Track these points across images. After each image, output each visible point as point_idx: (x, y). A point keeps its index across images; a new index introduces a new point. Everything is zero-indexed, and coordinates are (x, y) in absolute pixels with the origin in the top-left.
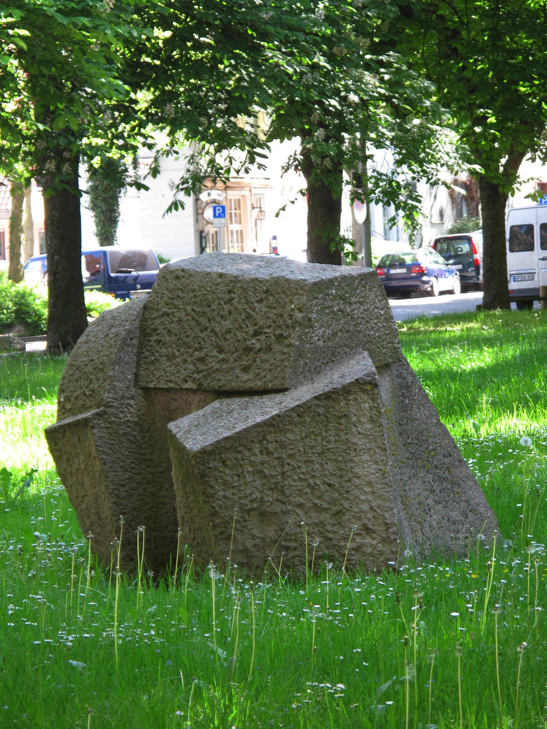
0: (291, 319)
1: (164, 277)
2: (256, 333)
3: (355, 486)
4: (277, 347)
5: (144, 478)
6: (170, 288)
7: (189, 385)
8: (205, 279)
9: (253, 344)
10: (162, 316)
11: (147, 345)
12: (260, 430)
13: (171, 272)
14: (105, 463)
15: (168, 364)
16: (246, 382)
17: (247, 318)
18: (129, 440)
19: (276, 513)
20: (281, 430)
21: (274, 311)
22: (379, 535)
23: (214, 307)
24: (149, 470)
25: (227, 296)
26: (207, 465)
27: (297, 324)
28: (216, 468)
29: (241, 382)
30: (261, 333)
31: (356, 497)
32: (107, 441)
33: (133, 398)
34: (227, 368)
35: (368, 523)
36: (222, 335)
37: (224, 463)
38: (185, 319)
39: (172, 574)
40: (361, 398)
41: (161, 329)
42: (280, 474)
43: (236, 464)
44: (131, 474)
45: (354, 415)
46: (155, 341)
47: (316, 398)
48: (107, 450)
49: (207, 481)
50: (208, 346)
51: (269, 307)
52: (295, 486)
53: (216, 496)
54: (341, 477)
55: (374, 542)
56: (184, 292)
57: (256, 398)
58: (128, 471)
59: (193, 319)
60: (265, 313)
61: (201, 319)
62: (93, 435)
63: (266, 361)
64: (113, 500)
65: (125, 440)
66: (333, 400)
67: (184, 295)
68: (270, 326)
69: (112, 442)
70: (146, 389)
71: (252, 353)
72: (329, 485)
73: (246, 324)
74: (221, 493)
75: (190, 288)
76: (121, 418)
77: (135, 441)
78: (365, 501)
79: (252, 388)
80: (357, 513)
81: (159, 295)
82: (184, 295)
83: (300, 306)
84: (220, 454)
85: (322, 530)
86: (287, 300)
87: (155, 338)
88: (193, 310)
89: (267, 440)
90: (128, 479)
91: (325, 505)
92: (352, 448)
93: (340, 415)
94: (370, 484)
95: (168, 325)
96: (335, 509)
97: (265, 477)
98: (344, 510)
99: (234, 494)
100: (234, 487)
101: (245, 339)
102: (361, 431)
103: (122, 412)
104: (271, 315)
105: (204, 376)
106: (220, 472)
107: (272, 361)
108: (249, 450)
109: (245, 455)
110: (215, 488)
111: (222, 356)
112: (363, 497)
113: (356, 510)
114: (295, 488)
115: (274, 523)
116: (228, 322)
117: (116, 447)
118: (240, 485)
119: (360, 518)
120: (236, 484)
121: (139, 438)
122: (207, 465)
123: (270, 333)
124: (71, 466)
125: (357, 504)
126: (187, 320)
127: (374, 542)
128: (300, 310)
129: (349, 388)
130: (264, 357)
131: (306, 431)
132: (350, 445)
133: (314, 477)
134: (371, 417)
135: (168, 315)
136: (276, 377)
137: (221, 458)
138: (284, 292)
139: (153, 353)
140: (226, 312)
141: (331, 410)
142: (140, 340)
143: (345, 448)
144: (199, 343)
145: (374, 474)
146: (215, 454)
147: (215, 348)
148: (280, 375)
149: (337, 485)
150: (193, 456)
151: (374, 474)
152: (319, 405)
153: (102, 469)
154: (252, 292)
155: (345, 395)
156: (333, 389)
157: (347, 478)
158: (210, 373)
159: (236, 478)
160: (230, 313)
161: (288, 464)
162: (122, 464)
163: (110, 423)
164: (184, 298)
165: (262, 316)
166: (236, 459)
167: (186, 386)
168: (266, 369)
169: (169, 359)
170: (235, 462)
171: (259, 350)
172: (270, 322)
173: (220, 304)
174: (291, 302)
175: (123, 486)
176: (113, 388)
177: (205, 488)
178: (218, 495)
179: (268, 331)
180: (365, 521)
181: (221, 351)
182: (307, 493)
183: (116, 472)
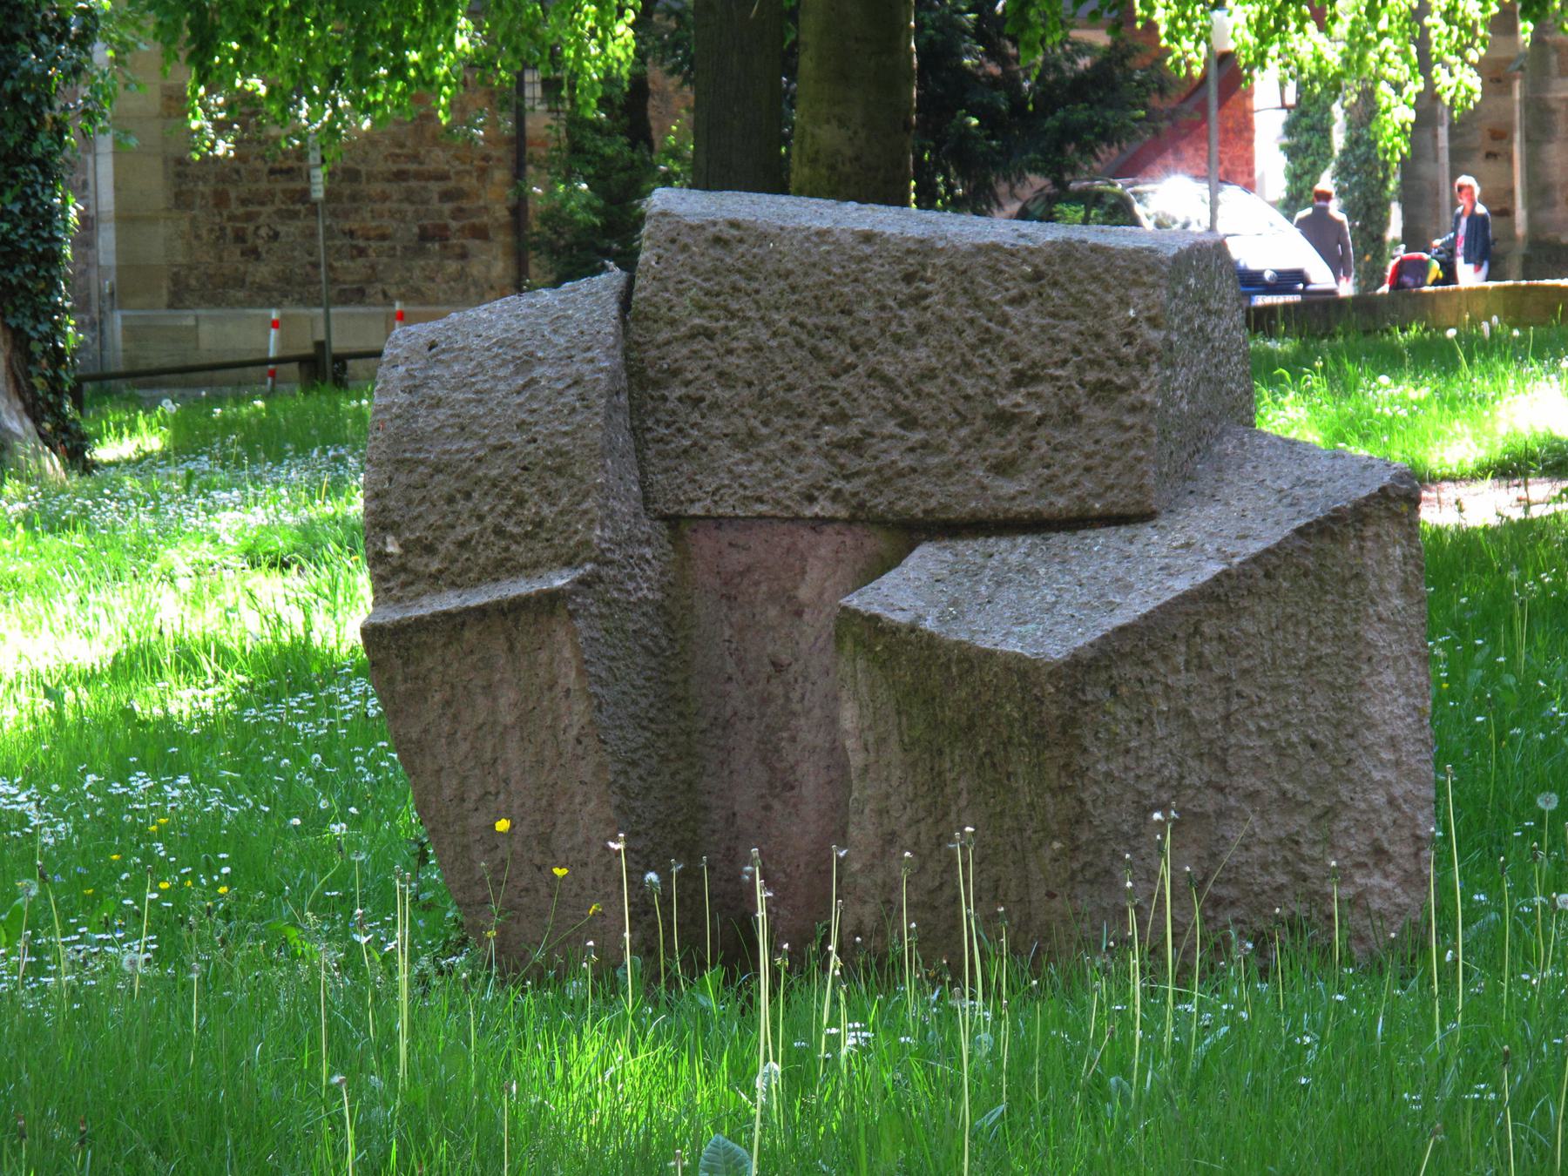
0: (1129, 343)
1: (673, 241)
2: (1020, 379)
3: (1365, 748)
4: (1094, 413)
5: (673, 745)
6: (702, 269)
7: (822, 507)
8: (817, 245)
9: (1017, 405)
10: (692, 336)
11: (655, 410)
12: (1191, 608)
13: (692, 228)
14: (599, 708)
15: (738, 456)
16: (1013, 498)
17: (983, 341)
18: (643, 647)
19: (1204, 816)
20: (1230, 611)
21: (1073, 325)
22: (1398, 867)
23: (863, 314)
24: (682, 724)
25: (904, 290)
26: (1080, 694)
27: (1153, 357)
28: (1097, 704)
29: (997, 498)
30: (1036, 379)
31: (1364, 775)
32: (603, 650)
33: (648, 542)
34: (943, 465)
35: (1383, 837)
36: (910, 383)
37: (1113, 690)
38: (774, 343)
39: (902, 981)
40: (1388, 534)
41: (693, 369)
42: (1222, 718)
43: (1139, 694)
44: (648, 735)
45: (1375, 575)
46: (680, 399)
47: (1299, 532)
48: (603, 674)
49: (1078, 737)
50: (866, 410)
51: (1053, 315)
52: (1250, 748)
53: (1090, 774)
54: (1338, 725)
55: (1388, 884)
56: (750, 279)
57: (1057, 539)
58: (644, 728)
59: (799, 344)
60: (1043, 329)
61: (826, 346)
62: (575, 633)
63: (1068, 447)
64: (615, 800)
65: (638, 649)
66: (1333, 537)
67: (755, 285)
68: (1065, 362)
69: (612, 653)
70: (673, 521)
71: (1016, 429)
72: (1314, 745)
73: (983, 356)
74: (1102, 767)
75: (770, 267)
76: (628, 592)
77: (657, 651)
78: (1379, 783)
79: (1039, 512)
80: (1363, 812)
81: (671, 286)
82: (755, 285)
83: (1153, 312)
84: (1107, 667)
85: (1290, 855)
86: (1110, 298)
87: (680, 391)
88: (793, 322)
89: (1202, 635)
90: (645, 747)
91: (1302, 795)
92: (1364, 656)
93: (1347, 575)
94: (1393, 743)
95: (716, 361)
96: (1321, 803)
97: (1190, 725)
98: (1339, 807)
99: (1127, 769)
100: (1127, 751)
101: (988, 394)
102: (1385, 615)
103: (632, 577)
104: (1063, 335)
105: (870, 485)
106: (1105, 713)
107: (1090, 447)
108: (1165, 658)
109: (1157, 672)
110: (1092, 754)
111: (917, 436)
112: (1377, 775)
113: (1363, 806)
114: (1249, 754)
115: (1195, 841)
116: (922, 353)
117: (621, 664)
118: (1141, 747)
119: (1367, 828)
120: (1133, 744)
121: (664, 642)
122: (1080, 694)
123: (1069, 379)
124: (455, 717)
125: (1364, 791)
126: (781, 346)
127: (1388, 884)
128: (1153, 322)
129: (1366, 510)
130: (1061, 437)
131: (1279, 611)
132: (1360, 647)
133: (1287, 724)
134: (1406, 581)
135: (709, 335)
136: (1111, 487)
137: (1111, 678)
138: (1095, 278)
139: (680, 430)
140: (911, 328)
141: (1329, 562)
142: (630, 397)
143: (1351, 654)
144: (833, 404)
145: (1401, 718)
146: (1098, 669)
147: (891, 415)
148: (1124, 480)
149: (1331, 747)
150: (1050, 674)
151: (1401, 718)
152: (1307, 551)
153: (591, 722)
154: (987, 278)
155: (1358, 525)
156: (1335, 510)
157: (1349, 729)
158: (886, 478)
159: (1135, 729)
160: (922, 329)
161: (1239, 695)
162: (632, 709)
163: (608, 604)
164: (757, 292)
165: (1035, 337)
166: (1140, 681)
167: (809, 511)
168: (1074, 466)
169: (740, 445)
170: (1138, 688)
171: (1041, 421)
172: (1061, 352)
173: (883, 308)
174: (1124, 303)
175: (634, 764)
176: (610, 516)
177: (1070, 755)
178: (1096, 771)
179: (1059, 372)
180: (1378, 833)
181: (909, 422)
182: (1269, 765)
183: (621, 728)
